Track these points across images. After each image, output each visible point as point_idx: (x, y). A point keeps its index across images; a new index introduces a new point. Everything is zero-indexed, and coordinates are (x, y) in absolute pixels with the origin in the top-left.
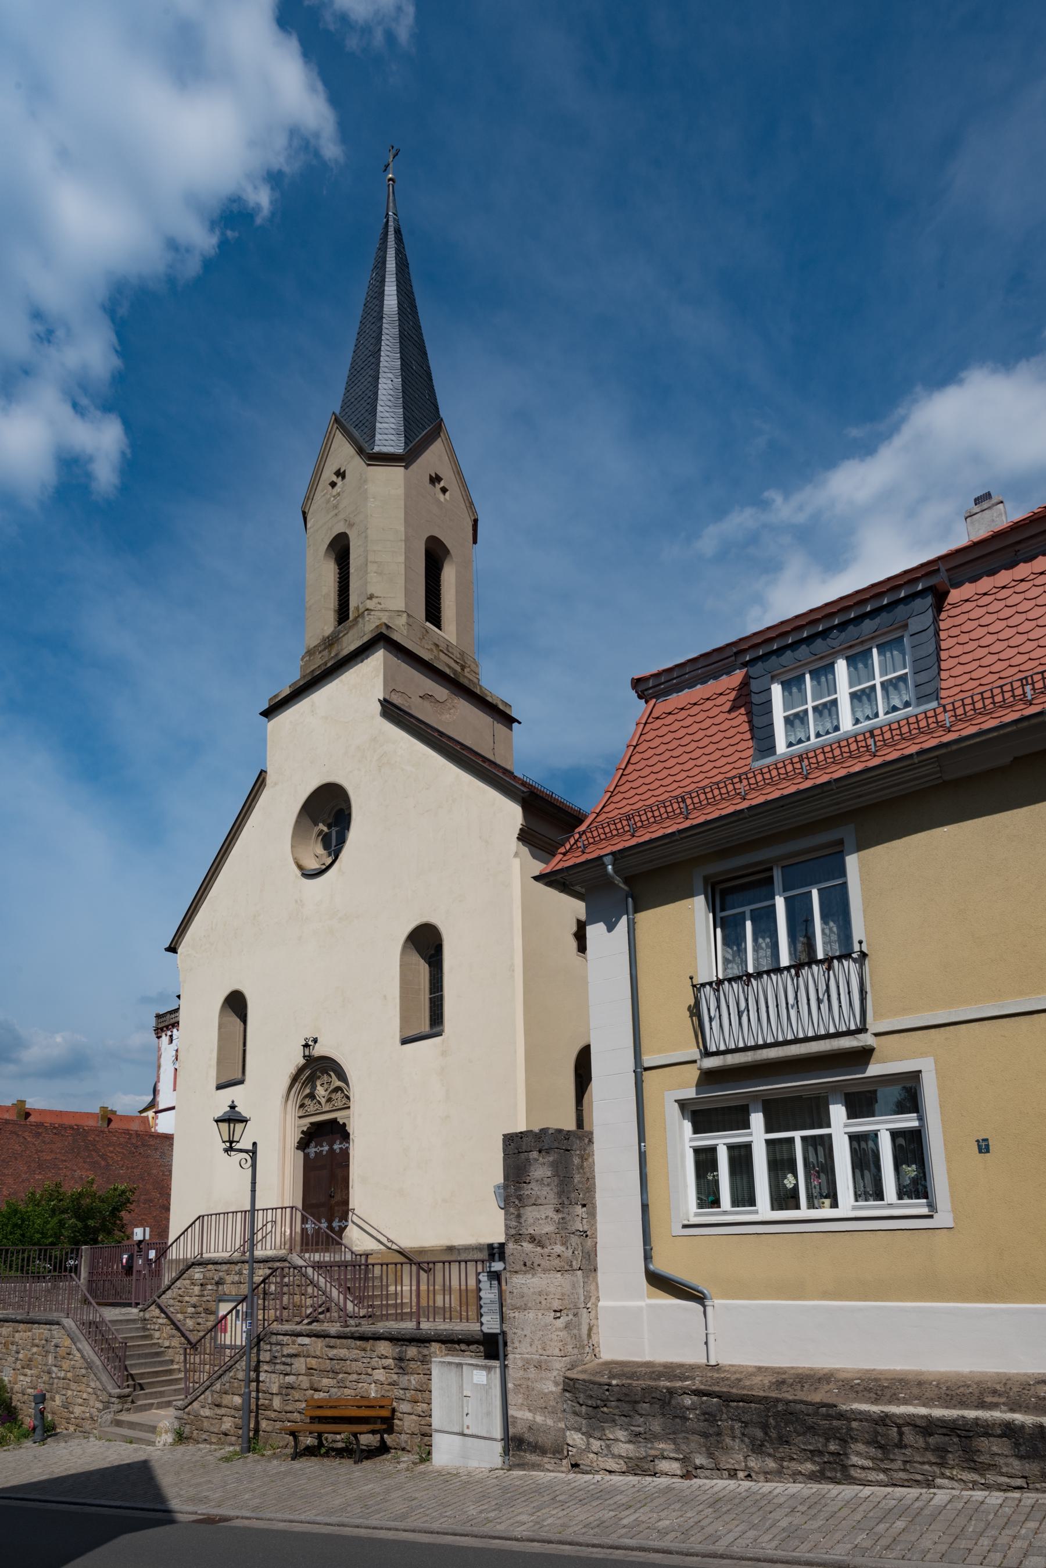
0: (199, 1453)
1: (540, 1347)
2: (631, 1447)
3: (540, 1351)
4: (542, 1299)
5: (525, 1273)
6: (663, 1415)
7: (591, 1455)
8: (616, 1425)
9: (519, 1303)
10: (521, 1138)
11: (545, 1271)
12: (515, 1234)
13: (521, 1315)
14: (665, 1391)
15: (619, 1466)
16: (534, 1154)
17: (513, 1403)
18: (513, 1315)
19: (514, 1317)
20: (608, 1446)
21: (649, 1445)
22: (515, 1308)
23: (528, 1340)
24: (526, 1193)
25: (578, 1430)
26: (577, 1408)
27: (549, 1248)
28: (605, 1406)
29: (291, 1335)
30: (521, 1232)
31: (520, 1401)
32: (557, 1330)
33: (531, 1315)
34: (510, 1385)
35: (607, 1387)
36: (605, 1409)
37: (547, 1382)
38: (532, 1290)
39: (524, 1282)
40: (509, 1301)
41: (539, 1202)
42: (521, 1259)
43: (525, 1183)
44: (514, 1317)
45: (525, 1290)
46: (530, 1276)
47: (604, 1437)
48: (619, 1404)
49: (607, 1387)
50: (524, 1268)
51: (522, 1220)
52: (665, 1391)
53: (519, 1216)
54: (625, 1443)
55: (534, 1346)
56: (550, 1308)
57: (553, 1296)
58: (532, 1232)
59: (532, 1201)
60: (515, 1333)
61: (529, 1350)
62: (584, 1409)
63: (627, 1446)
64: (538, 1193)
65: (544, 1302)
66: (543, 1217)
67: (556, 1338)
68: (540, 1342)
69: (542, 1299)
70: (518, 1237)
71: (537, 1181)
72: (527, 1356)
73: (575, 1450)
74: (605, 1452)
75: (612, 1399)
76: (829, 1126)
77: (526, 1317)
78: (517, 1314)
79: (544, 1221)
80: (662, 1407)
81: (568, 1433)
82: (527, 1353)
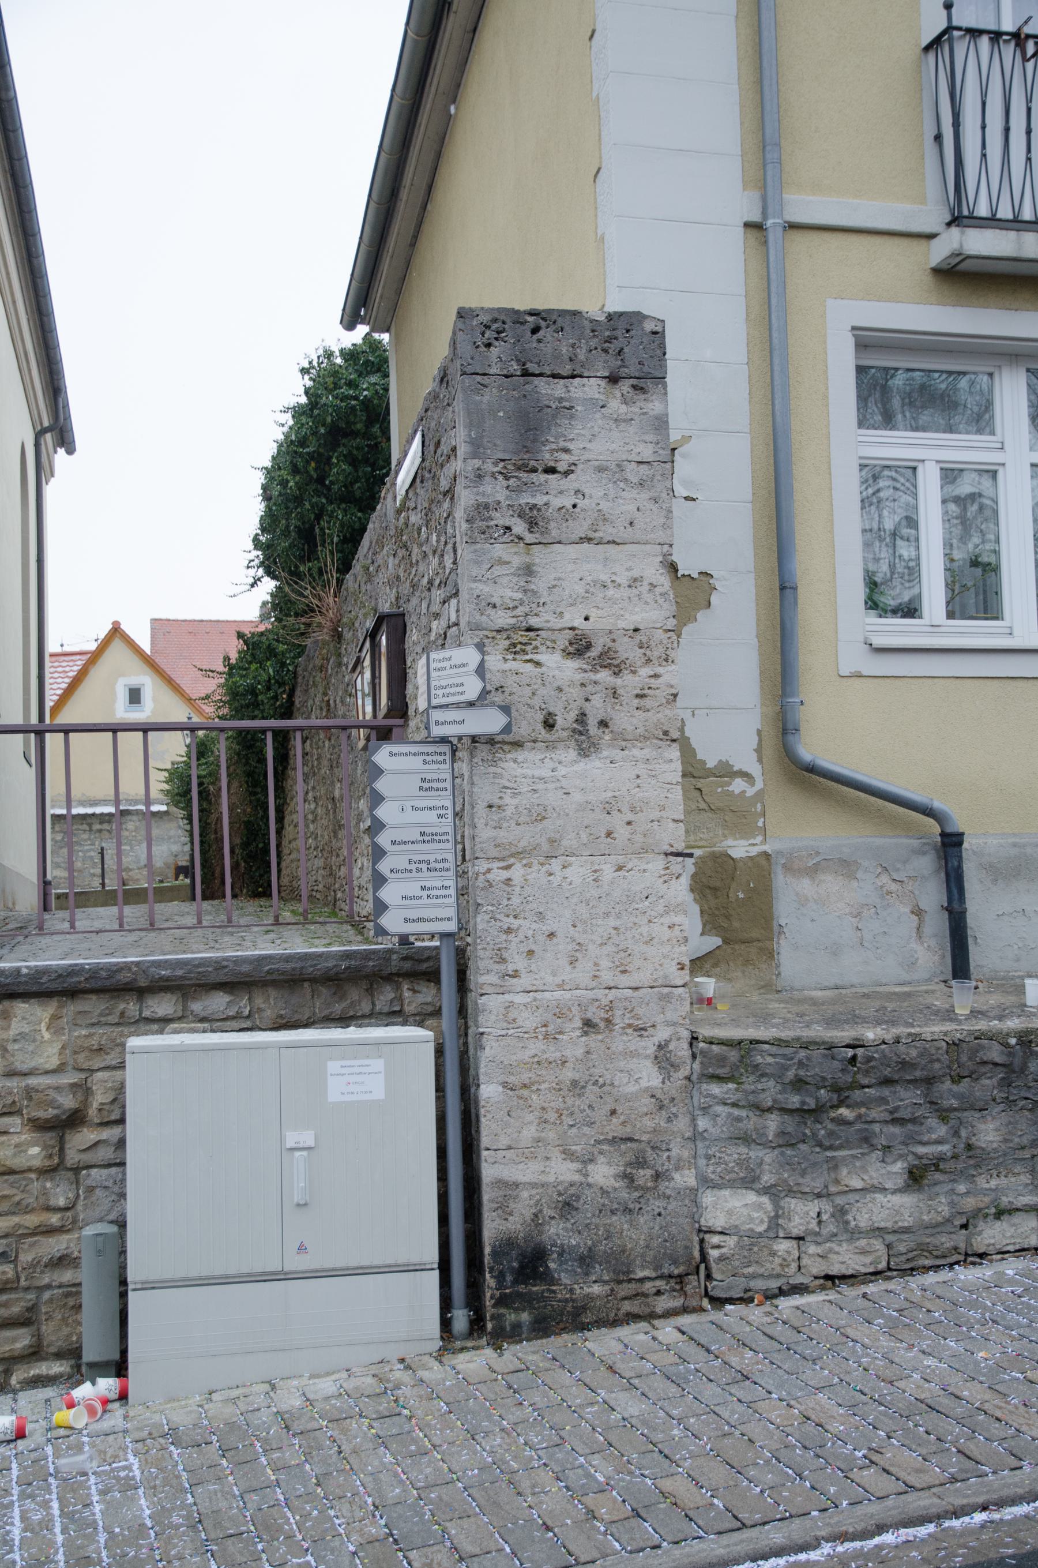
0: (662, 901)
1: (605, 963)
2: (907, 1201)
3: (607, 977)
4: (617, 822)
5: (550, 746)
6: (1009, 1102)
7: (783, 1246)
8: (873, 1147)
9: (524, 836)
10: (535, 330)
11: (623, 740)
12: (514, 628)
13: (537, 874)
14: (1013, 1041)
15: (868, 1260)
16: (591, 388)
17: (504, 1141)
18: (505, 874)
19: (508, 881)
20: (841, 1212)
21: (962, 1188)
22: (510, 855)
23: (563, 946)
24: (557, 502)
25: (749, 1181)
26: (751, 1122)
27: (645, 671)
28: (841, 1103)
29: (764, 166)
30: (534, 622)
31: (529, 1133)
32: (668, 910)
33: (577, 872)
34: (489, 1092)
35: (850, 1052)
36: (844, 1111)
37: (633, 1064)
38: (577, 797)
39: (545, 772)
40: (485, 833)
41: (606, 532)
42: (537, 702)
43: (551, 470)
44: (508, 881)
45: (552, 798)
46: (572, 754)
47: (833, 1189)
48: (886, 1092)
49: (850, 1052)
50: (543, 733)
51: (540, 584)
52: (1013, 1041)
53: (528, 571)
54: (894, 1192)
55: (585, 965)
56: (645, 850)
57: (656, 814)
58: (578, 622)
59: (581, 528)
60: (509, 931)
61: (566, 974)
62: (772, 1123)
63: (897, 1199)
64: (604, 506)
65: (622, 833)
66: (623, 579)
67: (667, 934)
68: (609, 949)
69: (617, 822)
70: (519, 637)
71: (601, 469)
72: (558, 994)
73: (731, 1241)
74: (831, 1228)
75: (865, 1081)
76: (235, 896)
77: (556, 880)
78: (517, 873)
79: (626, 592)
80: (1006, 1083)
81: (708, 1198)
82: (561, 987)
